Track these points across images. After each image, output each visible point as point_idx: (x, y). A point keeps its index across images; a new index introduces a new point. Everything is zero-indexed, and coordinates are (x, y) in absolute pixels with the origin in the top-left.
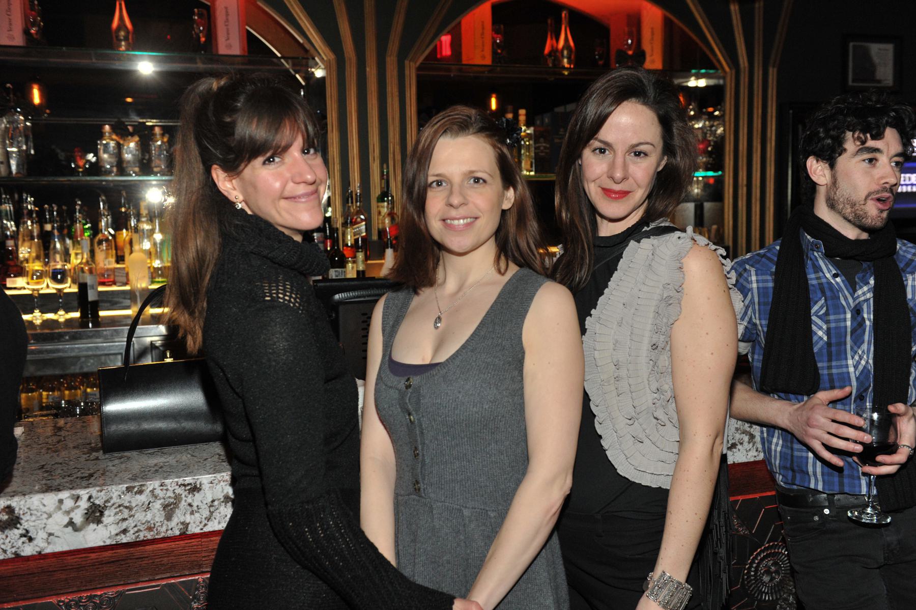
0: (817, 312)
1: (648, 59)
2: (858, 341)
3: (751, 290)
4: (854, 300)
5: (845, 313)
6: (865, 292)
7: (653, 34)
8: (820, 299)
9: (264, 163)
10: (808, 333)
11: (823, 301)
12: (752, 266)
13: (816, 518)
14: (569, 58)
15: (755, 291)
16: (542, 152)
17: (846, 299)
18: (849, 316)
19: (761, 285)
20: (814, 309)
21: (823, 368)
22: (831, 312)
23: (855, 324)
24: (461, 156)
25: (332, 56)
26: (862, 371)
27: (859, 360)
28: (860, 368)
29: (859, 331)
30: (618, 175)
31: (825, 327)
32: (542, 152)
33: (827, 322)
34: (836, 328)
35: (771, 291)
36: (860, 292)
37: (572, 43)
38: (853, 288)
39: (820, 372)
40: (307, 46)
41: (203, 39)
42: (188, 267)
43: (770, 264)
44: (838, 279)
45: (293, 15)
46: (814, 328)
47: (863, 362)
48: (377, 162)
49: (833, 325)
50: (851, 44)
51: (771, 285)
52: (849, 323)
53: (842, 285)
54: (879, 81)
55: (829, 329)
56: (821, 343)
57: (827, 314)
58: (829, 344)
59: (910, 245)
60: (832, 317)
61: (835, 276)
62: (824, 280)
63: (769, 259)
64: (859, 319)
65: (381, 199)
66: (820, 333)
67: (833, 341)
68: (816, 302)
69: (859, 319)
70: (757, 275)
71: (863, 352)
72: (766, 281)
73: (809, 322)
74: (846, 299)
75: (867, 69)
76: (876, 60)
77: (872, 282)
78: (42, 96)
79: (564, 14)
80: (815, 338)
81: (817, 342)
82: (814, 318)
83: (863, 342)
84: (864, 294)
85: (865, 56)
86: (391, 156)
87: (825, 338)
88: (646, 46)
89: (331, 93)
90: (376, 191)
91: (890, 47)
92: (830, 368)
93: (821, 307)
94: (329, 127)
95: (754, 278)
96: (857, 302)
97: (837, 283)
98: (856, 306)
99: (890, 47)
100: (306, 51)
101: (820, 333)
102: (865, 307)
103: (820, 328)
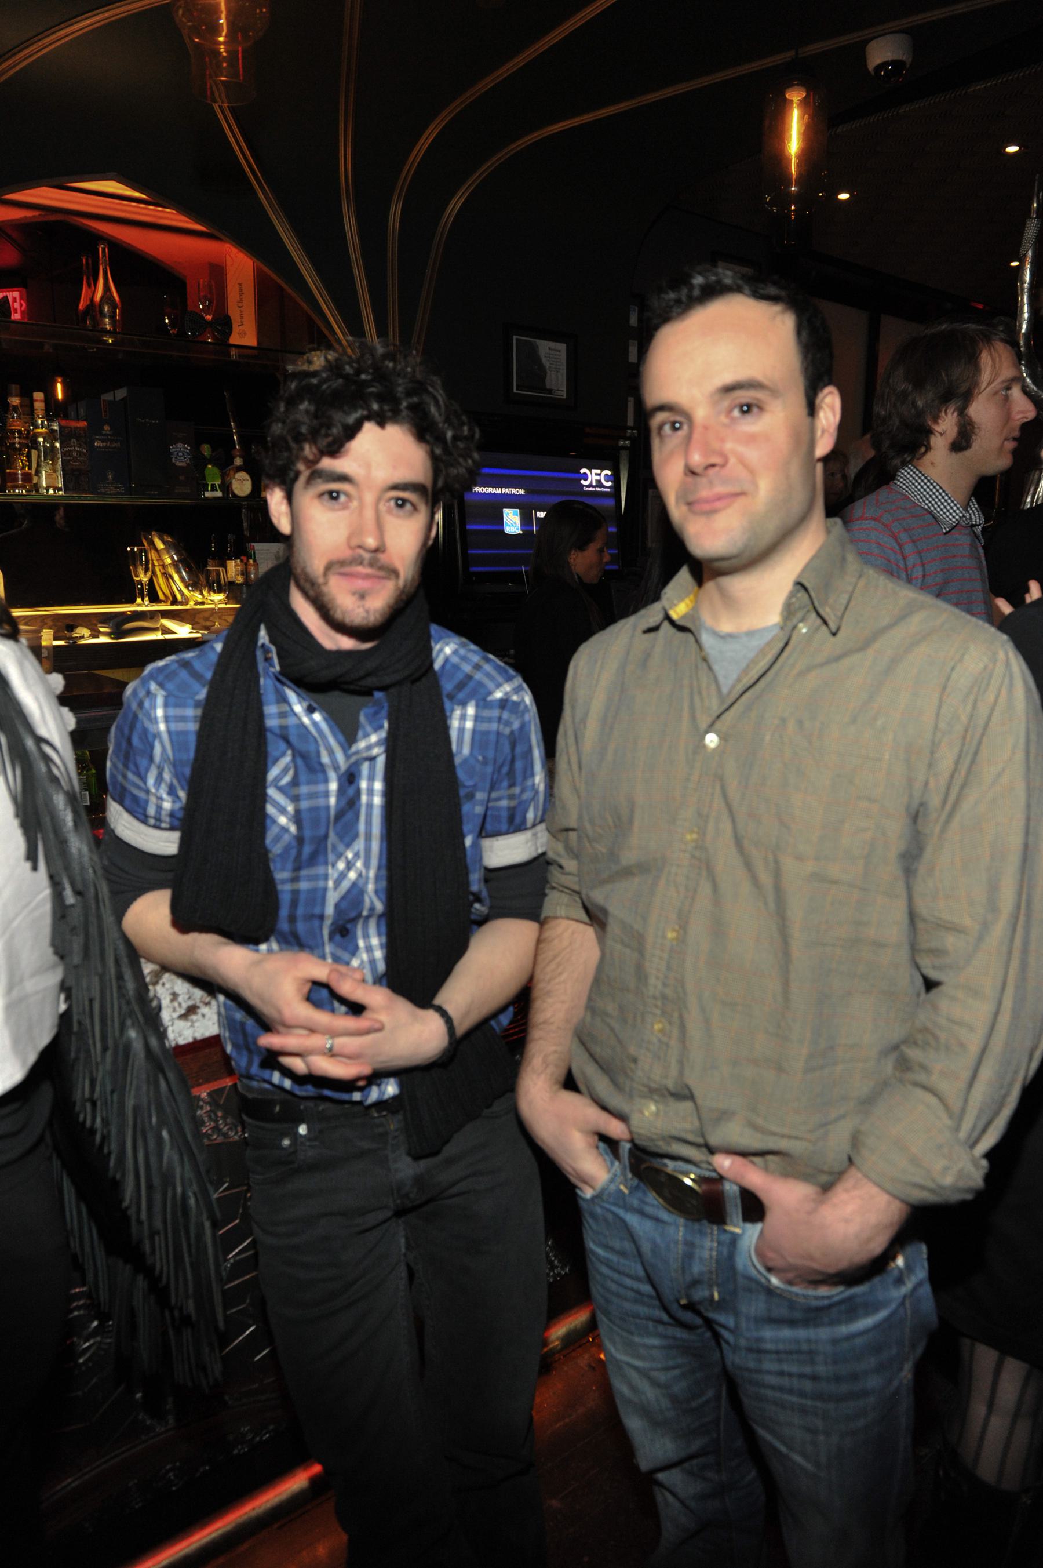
0: (278, 779)
1: (236, 329)
2: (348, 836)
3: (157, 735)
4: (348, 757)
5: (326, 781)
6: (372, 741)
7: (241, 293)
8: (283, 754)
9: (321, 495)
10: (259, 820)
11: (287, 759)
12: (161, 685)
13: (286, 1142)
14: (112, 317)
15: (165, 737)
16: (75, 460)
17: (331, 753)
18: (333, 786)
19: (173, 726)
20: (273, 773)
21: (283, 882)
22: (303, 778)
23: (343, 802)
26: (349, 891)
27: (356, 868)
28: (345, 885)
29: (349, 815)
31: (290, 808)
32: (75, 460)
33: (295, 799)
34: (311, 810)
35: (192, 740)
36: (362, 744)
38: (349, 734)
39: (279, 887)
43: (196, 685)
44: (317, 716)
46: (270, 809)
47: (352, 875)
49: (304, 804)
50: (515, 337)
51: (193, 727)
52: (333, 801)
53: (324, 726)
54: (550, 391)
55: (297, 812)
56: (286, 838)
57: (295, 782)
58: (300, 840)
59: (473, 647)
60: (304, 789)
61: (310, 710)
62: (291, 721)
63: (197, 676)
64: (351, 792)
66: (281, 816)
67: (307, 833)
68: (276, 760)
69: (351, 792)
70: (166, 705)
71: (357, 855)
72: (183, 719)
73: (262, 798)
74: (331, 753)
75: (535, 374)
76: (546, 362)
77: (386, 725)
80: (271, 833)
81: (277, 839)
82: (271, 792)
83: (356, 836)
84: (369, 747)
85: (531, 356)
87: (293, 829)
88: (233, 312)
91: (562, 347)
92: (295, 879)
93: (285, 771)
95: (160, 712)
96: (353, 759)
97: (315, 724)
98: (351, 766)
99: (562, 347)
101: (283, 820)
102: (365, 767)
103: (283, 811)
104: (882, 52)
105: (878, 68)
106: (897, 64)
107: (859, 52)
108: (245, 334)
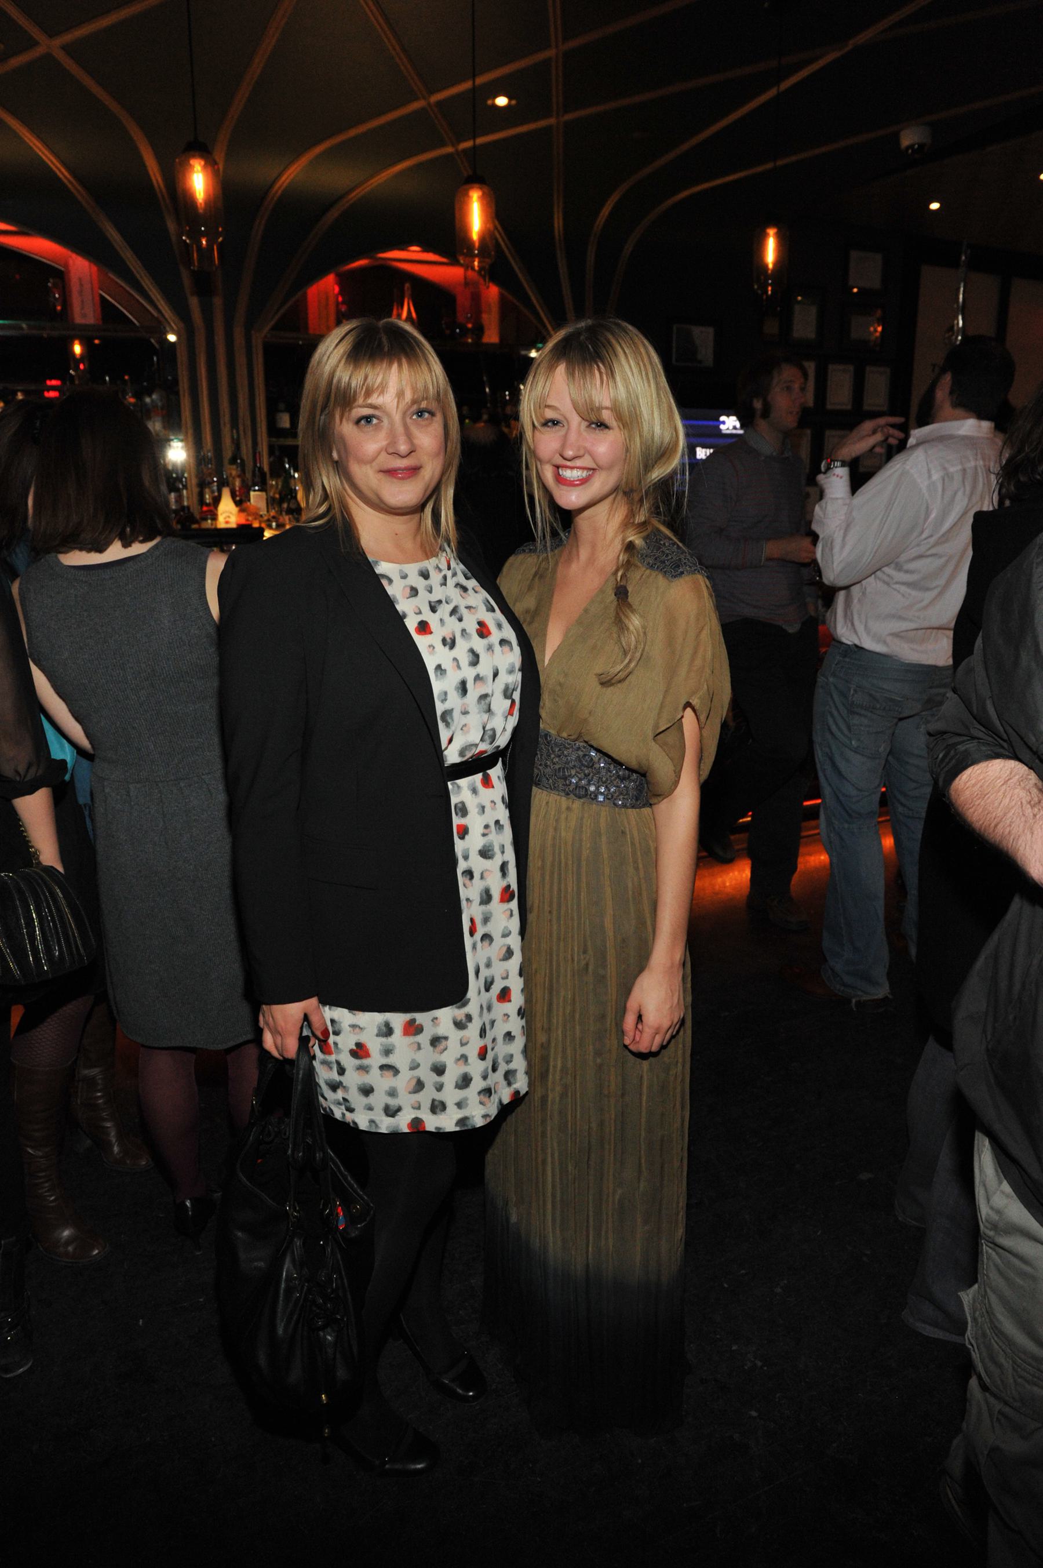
24: (186, 504)
25: (181, 325)
30: (403, 448)
37: (414, 315)
40: (161, 319)
41: (59, 308)
42: (616, 355)
45: (129, 269)
48: (228, 426)
54: (700, 362)
65: (233, 461)
78: (51, 399)
79: (407, 285)
86: (240, 421)
89: (182, 358)
90: (228, 454)
91: (711, 330)
94: (181, 393)
99: (711, 330)
100: (160, 322)
104: (909, 138)
105: (908, 148)
106: (921, 146)
107: (896, 137)
108: (492, 336)
